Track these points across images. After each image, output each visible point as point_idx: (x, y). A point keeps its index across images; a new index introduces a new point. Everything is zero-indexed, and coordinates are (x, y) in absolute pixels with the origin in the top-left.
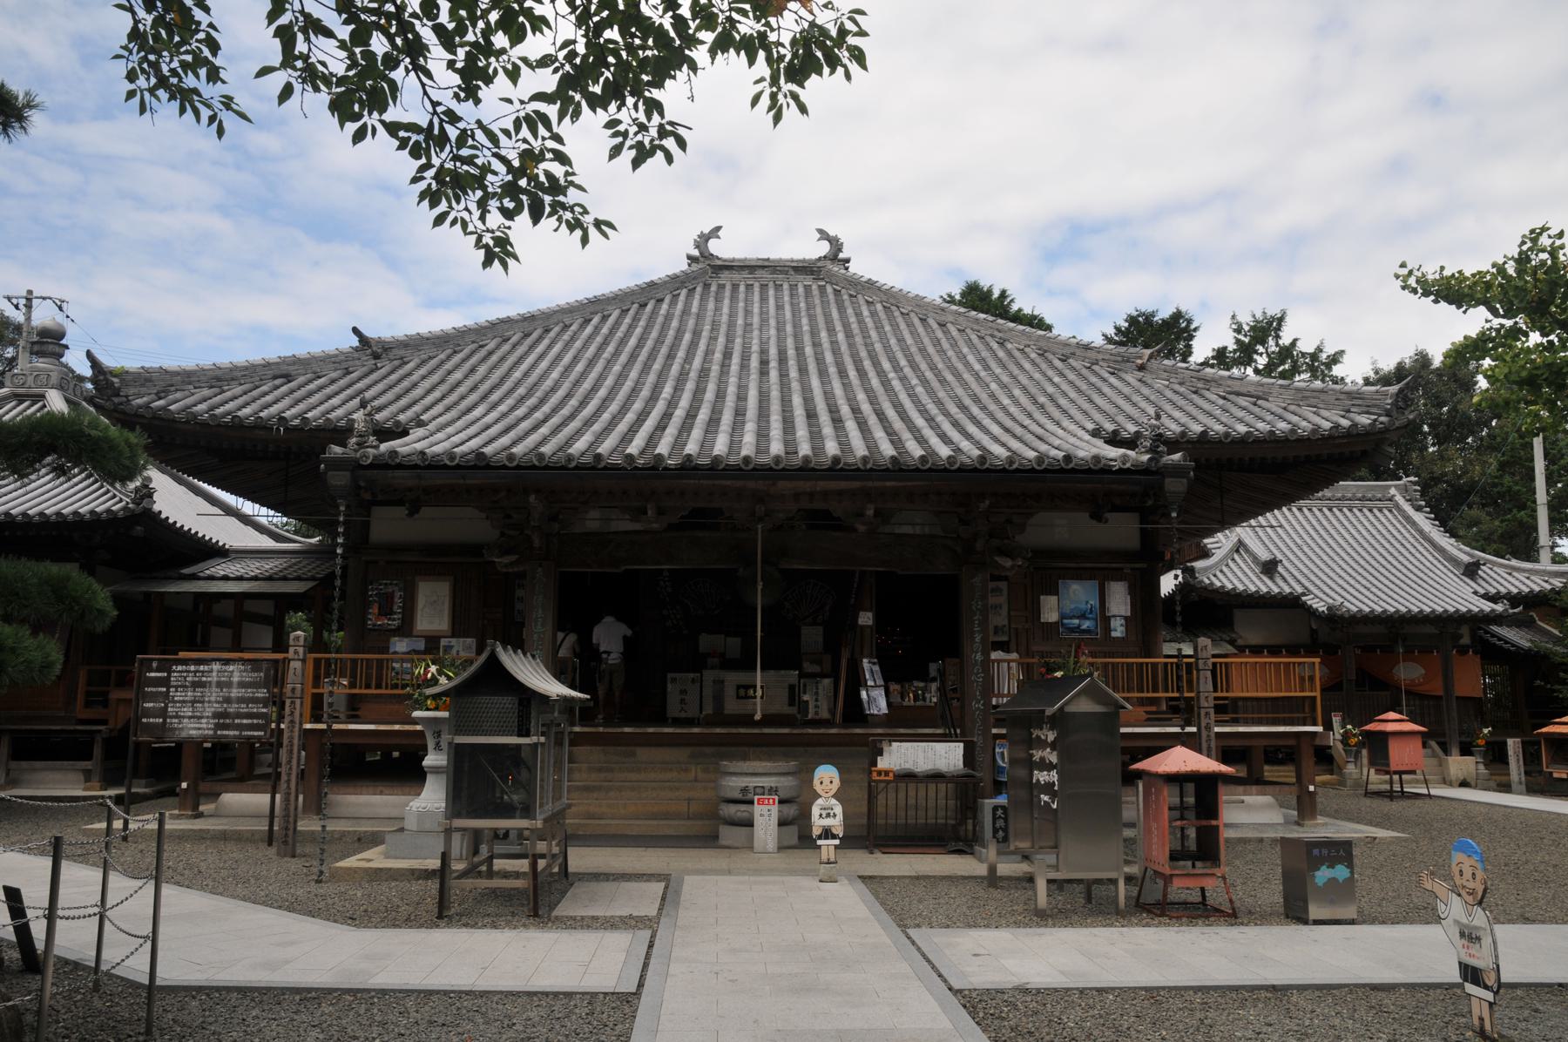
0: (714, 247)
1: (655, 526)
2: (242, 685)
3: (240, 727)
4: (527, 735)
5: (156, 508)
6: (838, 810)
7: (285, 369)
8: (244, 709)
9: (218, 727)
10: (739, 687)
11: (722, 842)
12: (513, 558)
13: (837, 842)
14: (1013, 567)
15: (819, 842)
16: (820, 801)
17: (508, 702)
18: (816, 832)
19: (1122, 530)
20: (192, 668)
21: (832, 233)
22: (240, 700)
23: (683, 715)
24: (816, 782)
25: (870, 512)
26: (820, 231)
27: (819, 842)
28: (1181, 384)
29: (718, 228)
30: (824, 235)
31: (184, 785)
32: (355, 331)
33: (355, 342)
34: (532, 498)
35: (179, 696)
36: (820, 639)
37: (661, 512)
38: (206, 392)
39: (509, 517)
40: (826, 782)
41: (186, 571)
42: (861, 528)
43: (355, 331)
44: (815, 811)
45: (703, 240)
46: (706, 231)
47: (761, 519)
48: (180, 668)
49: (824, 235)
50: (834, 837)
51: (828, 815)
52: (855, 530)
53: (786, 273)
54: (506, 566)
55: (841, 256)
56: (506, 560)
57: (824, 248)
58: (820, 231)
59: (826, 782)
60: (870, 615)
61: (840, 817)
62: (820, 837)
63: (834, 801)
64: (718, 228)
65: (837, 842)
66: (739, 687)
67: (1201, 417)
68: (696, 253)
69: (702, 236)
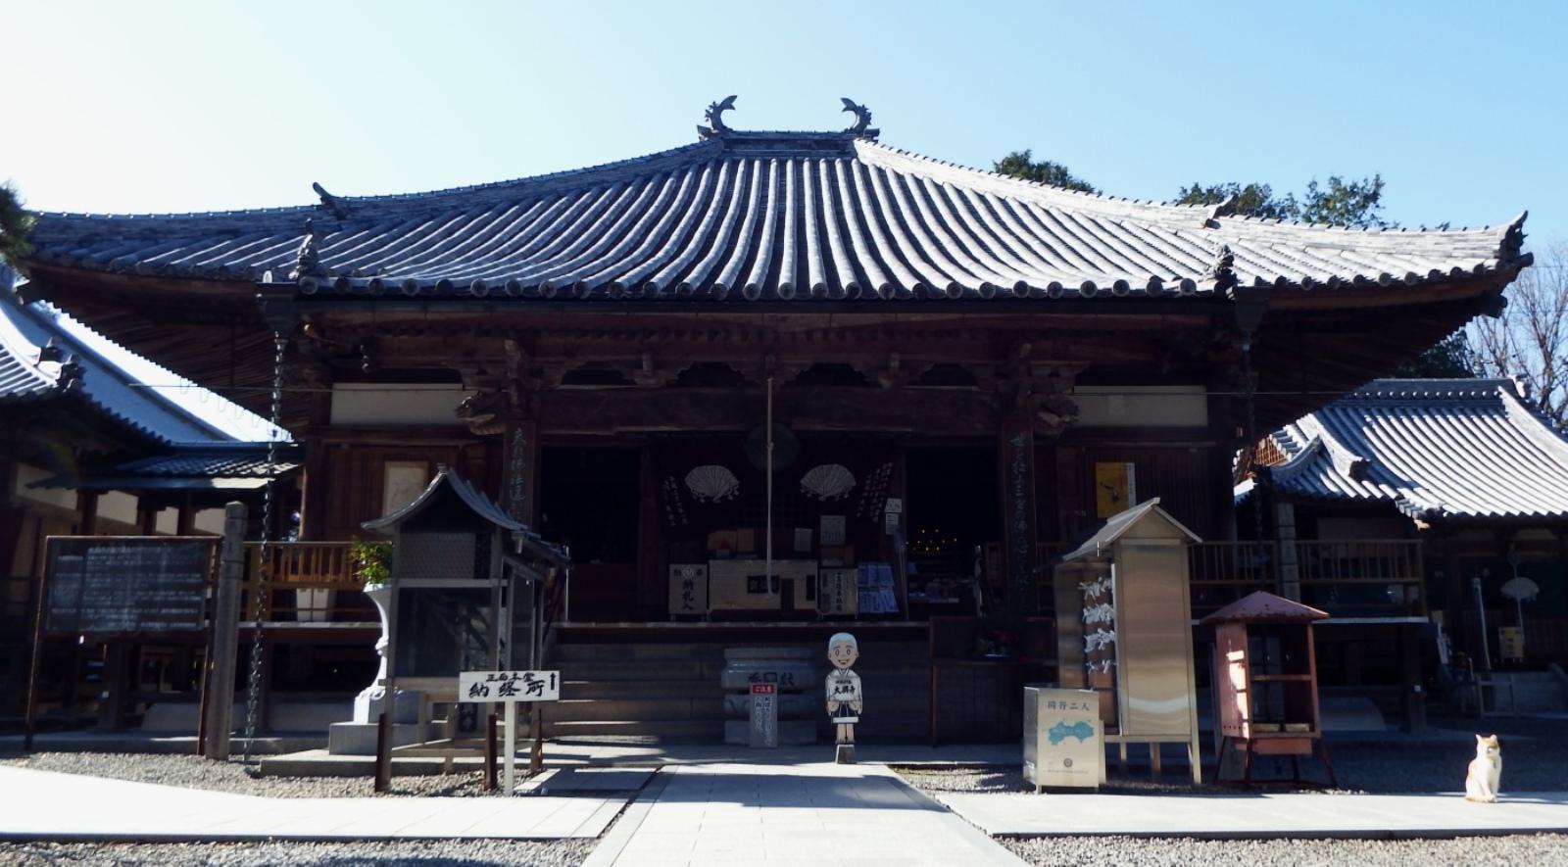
0: (728, 119)
1: (651, 381)
2: (170, 569)
3: (167, 618)
4: (486, 576)
5: (86, 390)
6: (857, 683)
7: (233, 224)
8: (172, 596)
9: (143, 618)
10: (750, 579)
11: (729, 739)
12: (489, 417)
13: (855, 719)
14: (1059, 425)
15: (836, 720)
16: (836, 673)
17: (465, 540)
18: (832, 707)
19: (1180, 407)
20: (113, 550)
21: (859, 103)
22: (168, 587)
23: (688, 612)
24: (831, 651)
25: (895, 364)
26: (845, 101)
27: (836, 720)
28: (1252, 240)
29: (733, 98)
30: (850, 105)
31: (105, 694)
32: (316, 187)
33: (316, 200)
34: (509, 344)
35: (95, 583)
36: (842, 530)
37: (657, 366)
38: (137, 243)
39: (482, 372)
40: (843, 650)
41: (121, 467)
42: (885, 383)
43: (316, 187)
44: (831, 684)
45: (715, 113)
46: (719, 102)
47: (771, 373)
48: (98, 550)
49: (850, 105)
50: (852, 714)
51: (845, 690)
52: (879, 385)
53: (809, 147)
54: (481, 427)
55: (869, 127)
56: (480, 419)
57: (851, 120)
58: (845, 101)
59: (843, 650)
60: (898, 501)
61: (858, 691)
62: (836, 714)
63: (852, 673)
64: (733, 98)
65: (855, 719)
66: (750, 579)
67: (1274, 268)
68: (709, 125)
69: (714, 106)
